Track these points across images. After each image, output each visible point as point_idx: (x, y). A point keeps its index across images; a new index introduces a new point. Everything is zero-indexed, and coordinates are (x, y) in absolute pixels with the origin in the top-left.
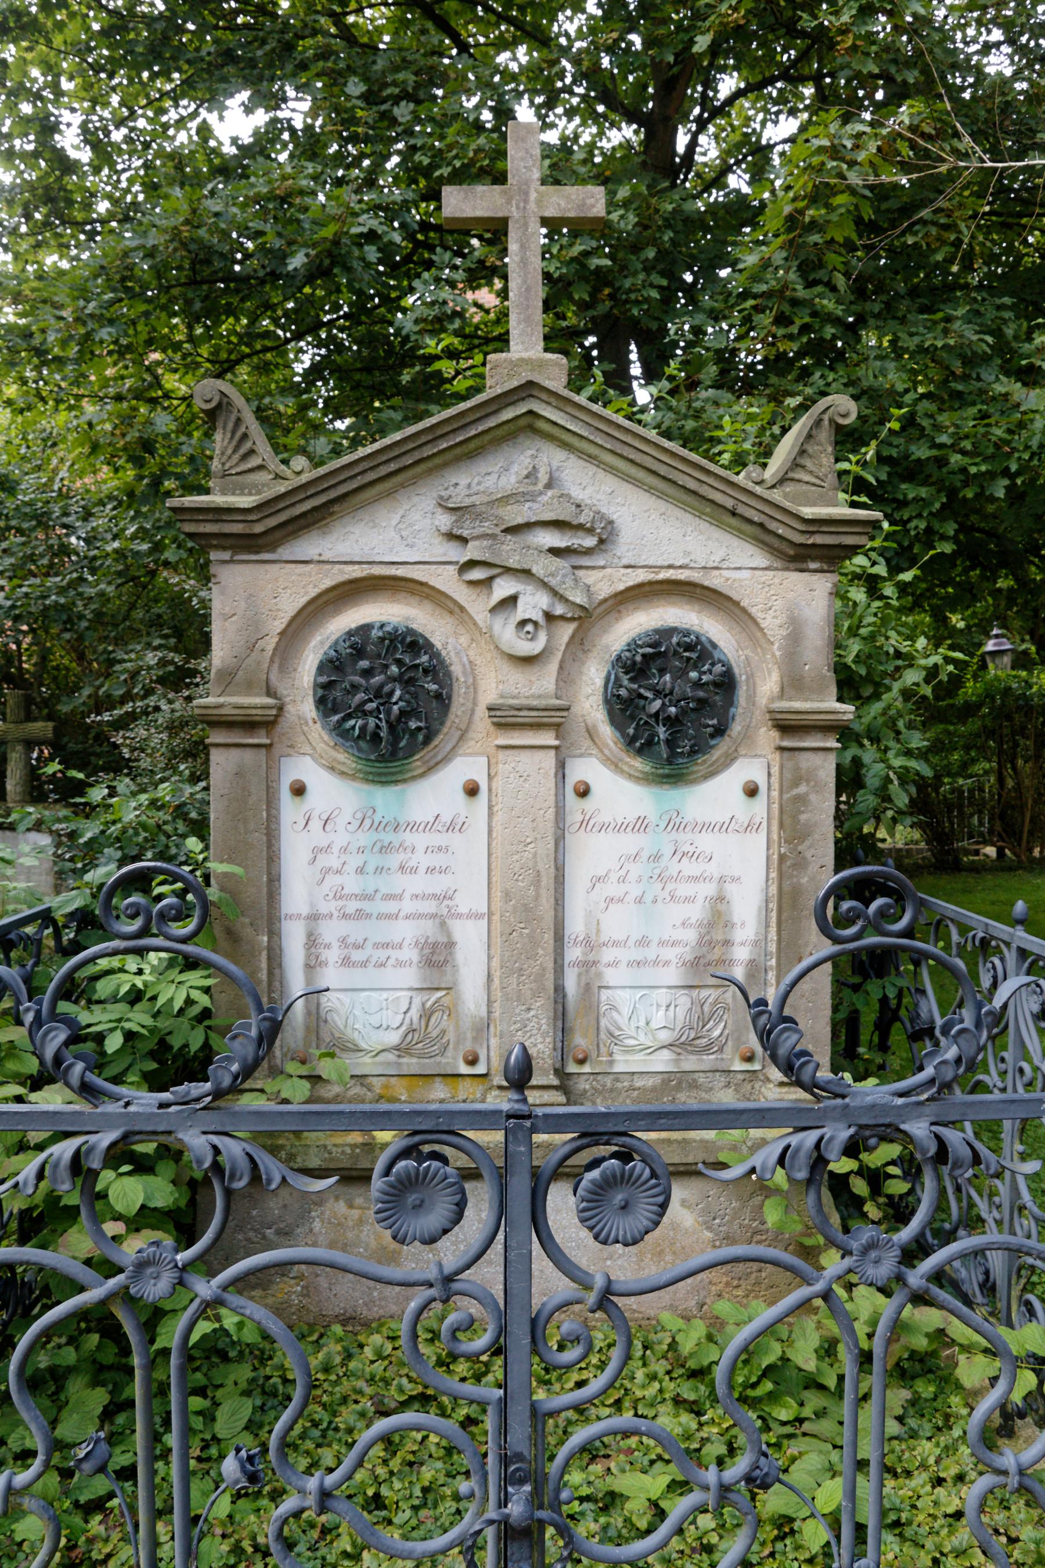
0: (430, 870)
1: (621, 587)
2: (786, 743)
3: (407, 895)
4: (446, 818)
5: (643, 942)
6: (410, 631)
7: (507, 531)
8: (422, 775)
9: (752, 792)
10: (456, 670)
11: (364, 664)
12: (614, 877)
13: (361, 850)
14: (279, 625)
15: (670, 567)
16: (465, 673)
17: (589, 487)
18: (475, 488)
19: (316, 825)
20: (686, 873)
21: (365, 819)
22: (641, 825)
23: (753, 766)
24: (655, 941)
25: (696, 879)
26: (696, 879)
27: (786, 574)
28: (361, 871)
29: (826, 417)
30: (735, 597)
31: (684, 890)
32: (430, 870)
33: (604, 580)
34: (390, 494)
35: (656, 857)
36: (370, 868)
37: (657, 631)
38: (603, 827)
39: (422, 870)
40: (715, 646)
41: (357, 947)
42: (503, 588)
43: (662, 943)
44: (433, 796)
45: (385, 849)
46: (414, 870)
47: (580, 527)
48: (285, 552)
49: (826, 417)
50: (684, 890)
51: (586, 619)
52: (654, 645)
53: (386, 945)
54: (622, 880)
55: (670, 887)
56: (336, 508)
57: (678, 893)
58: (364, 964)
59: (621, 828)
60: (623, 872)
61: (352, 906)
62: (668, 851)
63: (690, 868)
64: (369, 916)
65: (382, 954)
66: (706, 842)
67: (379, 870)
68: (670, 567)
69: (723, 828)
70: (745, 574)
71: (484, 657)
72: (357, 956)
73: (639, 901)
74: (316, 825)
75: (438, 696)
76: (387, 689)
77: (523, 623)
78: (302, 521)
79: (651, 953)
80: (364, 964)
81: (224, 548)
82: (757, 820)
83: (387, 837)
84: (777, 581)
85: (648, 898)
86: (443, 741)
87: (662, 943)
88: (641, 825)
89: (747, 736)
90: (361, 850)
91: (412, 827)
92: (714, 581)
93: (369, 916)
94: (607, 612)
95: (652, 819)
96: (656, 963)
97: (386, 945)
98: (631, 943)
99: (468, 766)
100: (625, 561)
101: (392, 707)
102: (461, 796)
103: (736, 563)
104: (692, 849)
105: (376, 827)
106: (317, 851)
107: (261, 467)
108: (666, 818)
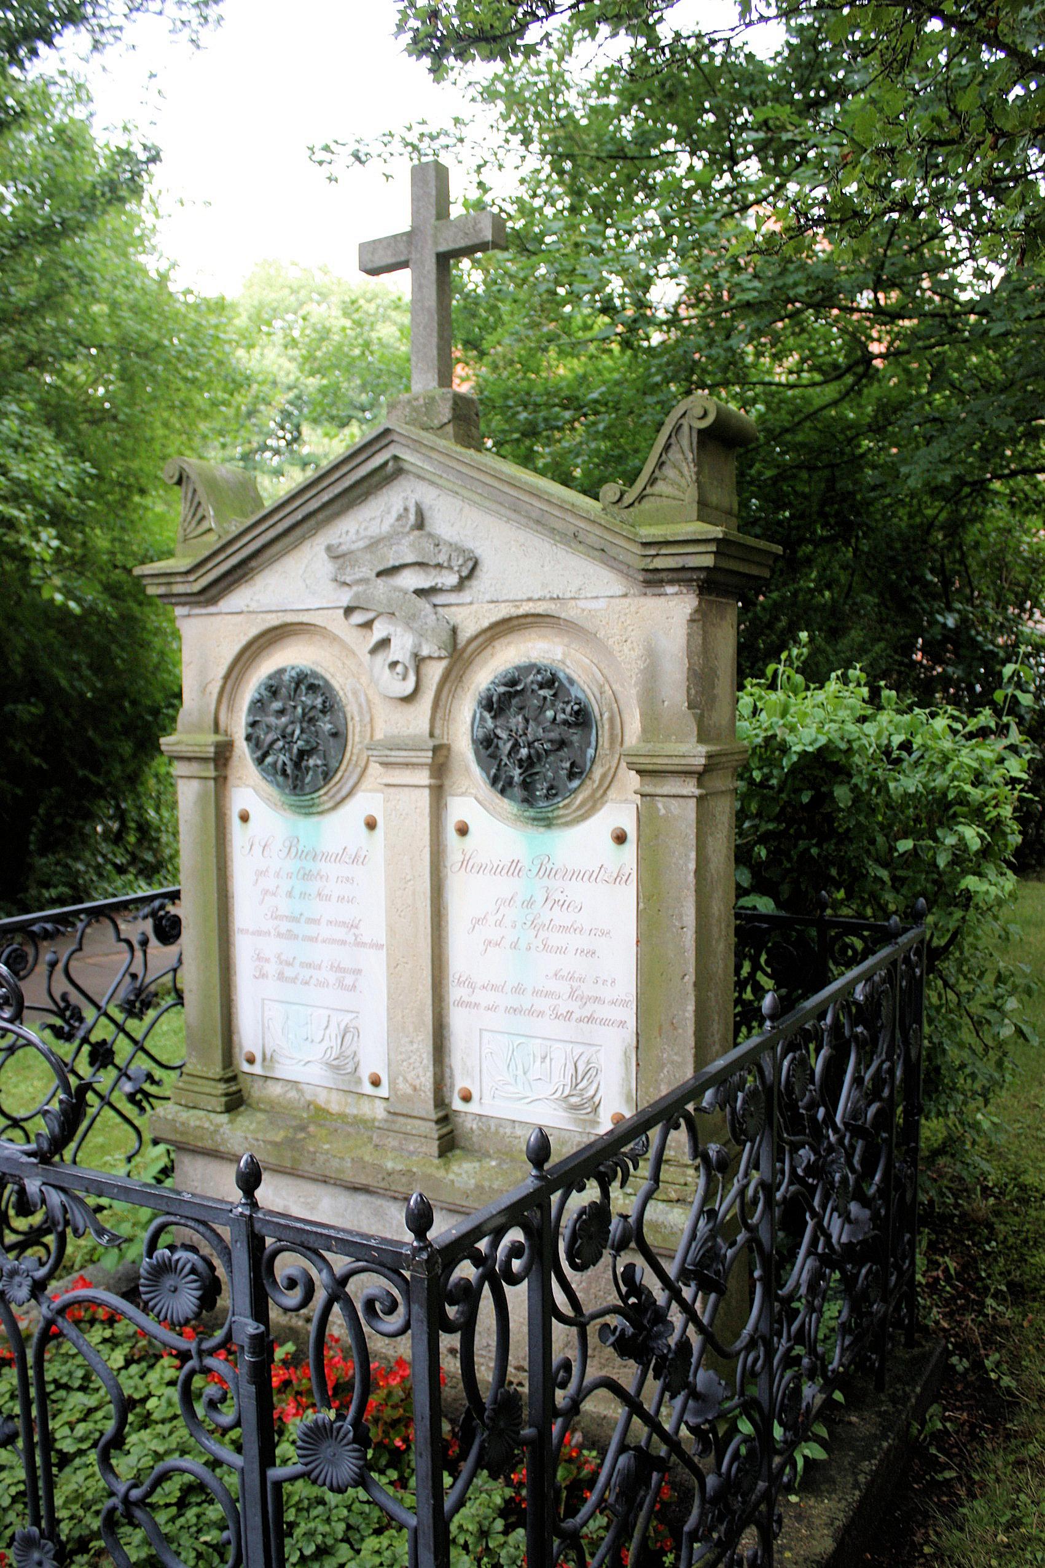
0: (341, 899)
1: (486, 624)
2: (648, 789)
3: (324, 921)
4: (352, 851)
5: (519, 990)
6: (315, 675)
7: (379, 574)
8: (334, 808)
9: (620, 838)
10: (352, 708)
11: (277, 705)
12: (491, 920)
13: (289, 876)
14: (222, 670)
15: (530, 599)
16: (361, 713)
17: (458, 521)
18: (362, 533)
19: (258, 849)
20: (557, 922)
21: (293, 848)
22: (514, 868)
23: (620, 811)
24: (530, 991)
25: (564, 929)
26: (564, 929)
27: (643, 600)
28: (290, 894)
29: (685, 422)
30: (588, 626)
31: (556, 939)
32: (341, 899)
33: (472, 614)
34: (296, 546)
35: (530, 903)
36: (296, 893)
37: (518, 668)
38: (481, 868)
39: (334, 899)
40: (572, 682)
41: (289, 964)
42: (380, 630)
43: (535, 992)
44: (339, 827)
45: (307, 876)
46: (328, 898)
47: (439, 566)
48: (225, 605)
49: (685, 422)
50: (556, 939)
51: (459, 655)
52: (513, 683)
53: (309, 965)
54: (499, 923)
55: (543, 934)
56: (253, 564)
57: (550, 943)
58: (294, 980)
59: (496, 871)
60: (499, 916)
61: (284, 926)
62: (540, 898)
63: (561, 917)
64: (296, 937)
65: (306, 973)
66: (576, 891)
67: (303, 895)
68: (530, 599)
69: (591, 877)
70: (601, 604)
71: (373, 693)
72: (289, 972)
73: (514, 946)
74: (258, 849)
75: (335, 735)
76: (289, 730)
77: (394, 664)
78: (230, 579)
79: (526, 1001)
80: (294, 980)
81: (184, 604)
82: (627, 871)
83: (309, 865)
84: (633, 609)
85: (522, 944)
86: (346, 775)
87: (535, 992)
88: (514, 868)
89: (609, 781)
90: (289, 876)
91: (326, 857)
92: (570, 612)
93: (296, 937)
94: (482, 648)
95: (525, 863)
96: (530, 1012)
97: (309, 965)
98: (508, 988)
99: (366, 801)
100: (488, 597)
101: (305, 744)
102: (611, 844)
103: (595, 590)
104: (562, 898)
105: (301, 855)
106: (260, 873)
107: (210, 530)
108: (537, 862)
